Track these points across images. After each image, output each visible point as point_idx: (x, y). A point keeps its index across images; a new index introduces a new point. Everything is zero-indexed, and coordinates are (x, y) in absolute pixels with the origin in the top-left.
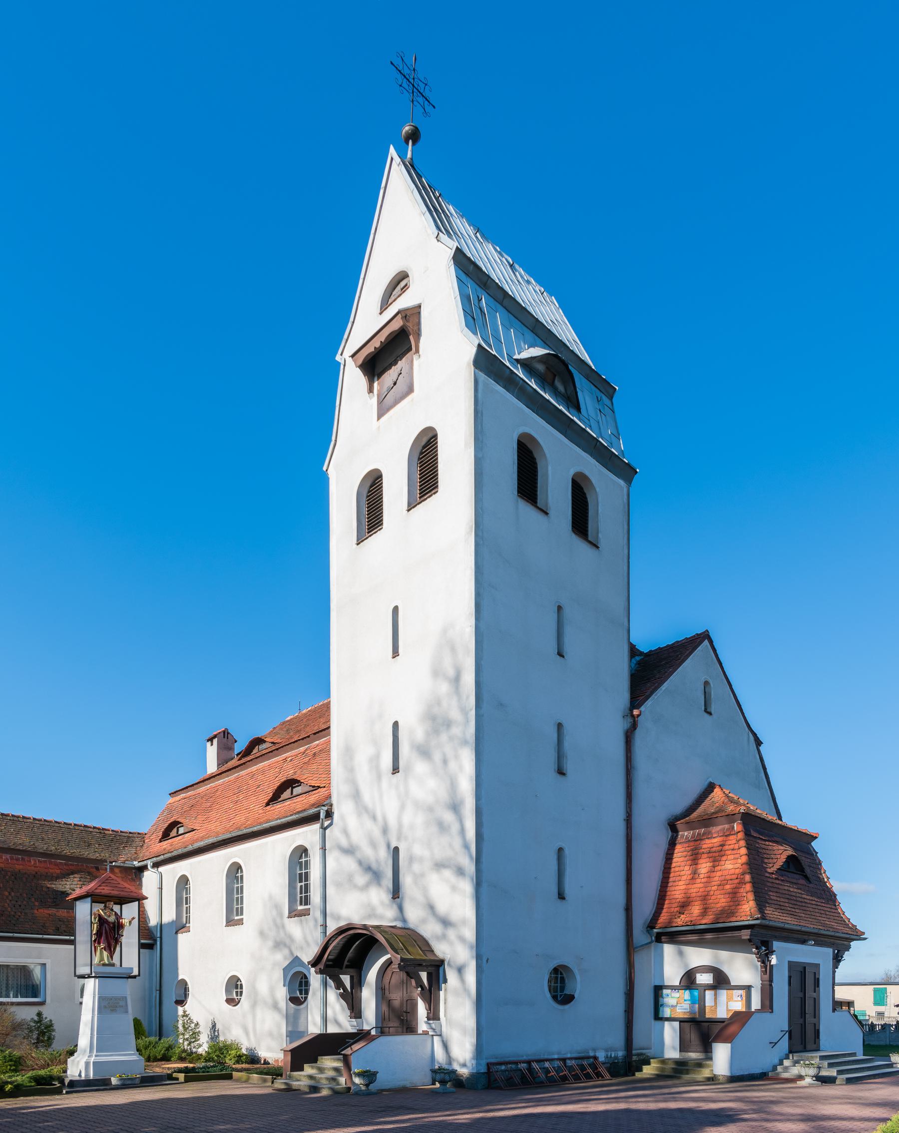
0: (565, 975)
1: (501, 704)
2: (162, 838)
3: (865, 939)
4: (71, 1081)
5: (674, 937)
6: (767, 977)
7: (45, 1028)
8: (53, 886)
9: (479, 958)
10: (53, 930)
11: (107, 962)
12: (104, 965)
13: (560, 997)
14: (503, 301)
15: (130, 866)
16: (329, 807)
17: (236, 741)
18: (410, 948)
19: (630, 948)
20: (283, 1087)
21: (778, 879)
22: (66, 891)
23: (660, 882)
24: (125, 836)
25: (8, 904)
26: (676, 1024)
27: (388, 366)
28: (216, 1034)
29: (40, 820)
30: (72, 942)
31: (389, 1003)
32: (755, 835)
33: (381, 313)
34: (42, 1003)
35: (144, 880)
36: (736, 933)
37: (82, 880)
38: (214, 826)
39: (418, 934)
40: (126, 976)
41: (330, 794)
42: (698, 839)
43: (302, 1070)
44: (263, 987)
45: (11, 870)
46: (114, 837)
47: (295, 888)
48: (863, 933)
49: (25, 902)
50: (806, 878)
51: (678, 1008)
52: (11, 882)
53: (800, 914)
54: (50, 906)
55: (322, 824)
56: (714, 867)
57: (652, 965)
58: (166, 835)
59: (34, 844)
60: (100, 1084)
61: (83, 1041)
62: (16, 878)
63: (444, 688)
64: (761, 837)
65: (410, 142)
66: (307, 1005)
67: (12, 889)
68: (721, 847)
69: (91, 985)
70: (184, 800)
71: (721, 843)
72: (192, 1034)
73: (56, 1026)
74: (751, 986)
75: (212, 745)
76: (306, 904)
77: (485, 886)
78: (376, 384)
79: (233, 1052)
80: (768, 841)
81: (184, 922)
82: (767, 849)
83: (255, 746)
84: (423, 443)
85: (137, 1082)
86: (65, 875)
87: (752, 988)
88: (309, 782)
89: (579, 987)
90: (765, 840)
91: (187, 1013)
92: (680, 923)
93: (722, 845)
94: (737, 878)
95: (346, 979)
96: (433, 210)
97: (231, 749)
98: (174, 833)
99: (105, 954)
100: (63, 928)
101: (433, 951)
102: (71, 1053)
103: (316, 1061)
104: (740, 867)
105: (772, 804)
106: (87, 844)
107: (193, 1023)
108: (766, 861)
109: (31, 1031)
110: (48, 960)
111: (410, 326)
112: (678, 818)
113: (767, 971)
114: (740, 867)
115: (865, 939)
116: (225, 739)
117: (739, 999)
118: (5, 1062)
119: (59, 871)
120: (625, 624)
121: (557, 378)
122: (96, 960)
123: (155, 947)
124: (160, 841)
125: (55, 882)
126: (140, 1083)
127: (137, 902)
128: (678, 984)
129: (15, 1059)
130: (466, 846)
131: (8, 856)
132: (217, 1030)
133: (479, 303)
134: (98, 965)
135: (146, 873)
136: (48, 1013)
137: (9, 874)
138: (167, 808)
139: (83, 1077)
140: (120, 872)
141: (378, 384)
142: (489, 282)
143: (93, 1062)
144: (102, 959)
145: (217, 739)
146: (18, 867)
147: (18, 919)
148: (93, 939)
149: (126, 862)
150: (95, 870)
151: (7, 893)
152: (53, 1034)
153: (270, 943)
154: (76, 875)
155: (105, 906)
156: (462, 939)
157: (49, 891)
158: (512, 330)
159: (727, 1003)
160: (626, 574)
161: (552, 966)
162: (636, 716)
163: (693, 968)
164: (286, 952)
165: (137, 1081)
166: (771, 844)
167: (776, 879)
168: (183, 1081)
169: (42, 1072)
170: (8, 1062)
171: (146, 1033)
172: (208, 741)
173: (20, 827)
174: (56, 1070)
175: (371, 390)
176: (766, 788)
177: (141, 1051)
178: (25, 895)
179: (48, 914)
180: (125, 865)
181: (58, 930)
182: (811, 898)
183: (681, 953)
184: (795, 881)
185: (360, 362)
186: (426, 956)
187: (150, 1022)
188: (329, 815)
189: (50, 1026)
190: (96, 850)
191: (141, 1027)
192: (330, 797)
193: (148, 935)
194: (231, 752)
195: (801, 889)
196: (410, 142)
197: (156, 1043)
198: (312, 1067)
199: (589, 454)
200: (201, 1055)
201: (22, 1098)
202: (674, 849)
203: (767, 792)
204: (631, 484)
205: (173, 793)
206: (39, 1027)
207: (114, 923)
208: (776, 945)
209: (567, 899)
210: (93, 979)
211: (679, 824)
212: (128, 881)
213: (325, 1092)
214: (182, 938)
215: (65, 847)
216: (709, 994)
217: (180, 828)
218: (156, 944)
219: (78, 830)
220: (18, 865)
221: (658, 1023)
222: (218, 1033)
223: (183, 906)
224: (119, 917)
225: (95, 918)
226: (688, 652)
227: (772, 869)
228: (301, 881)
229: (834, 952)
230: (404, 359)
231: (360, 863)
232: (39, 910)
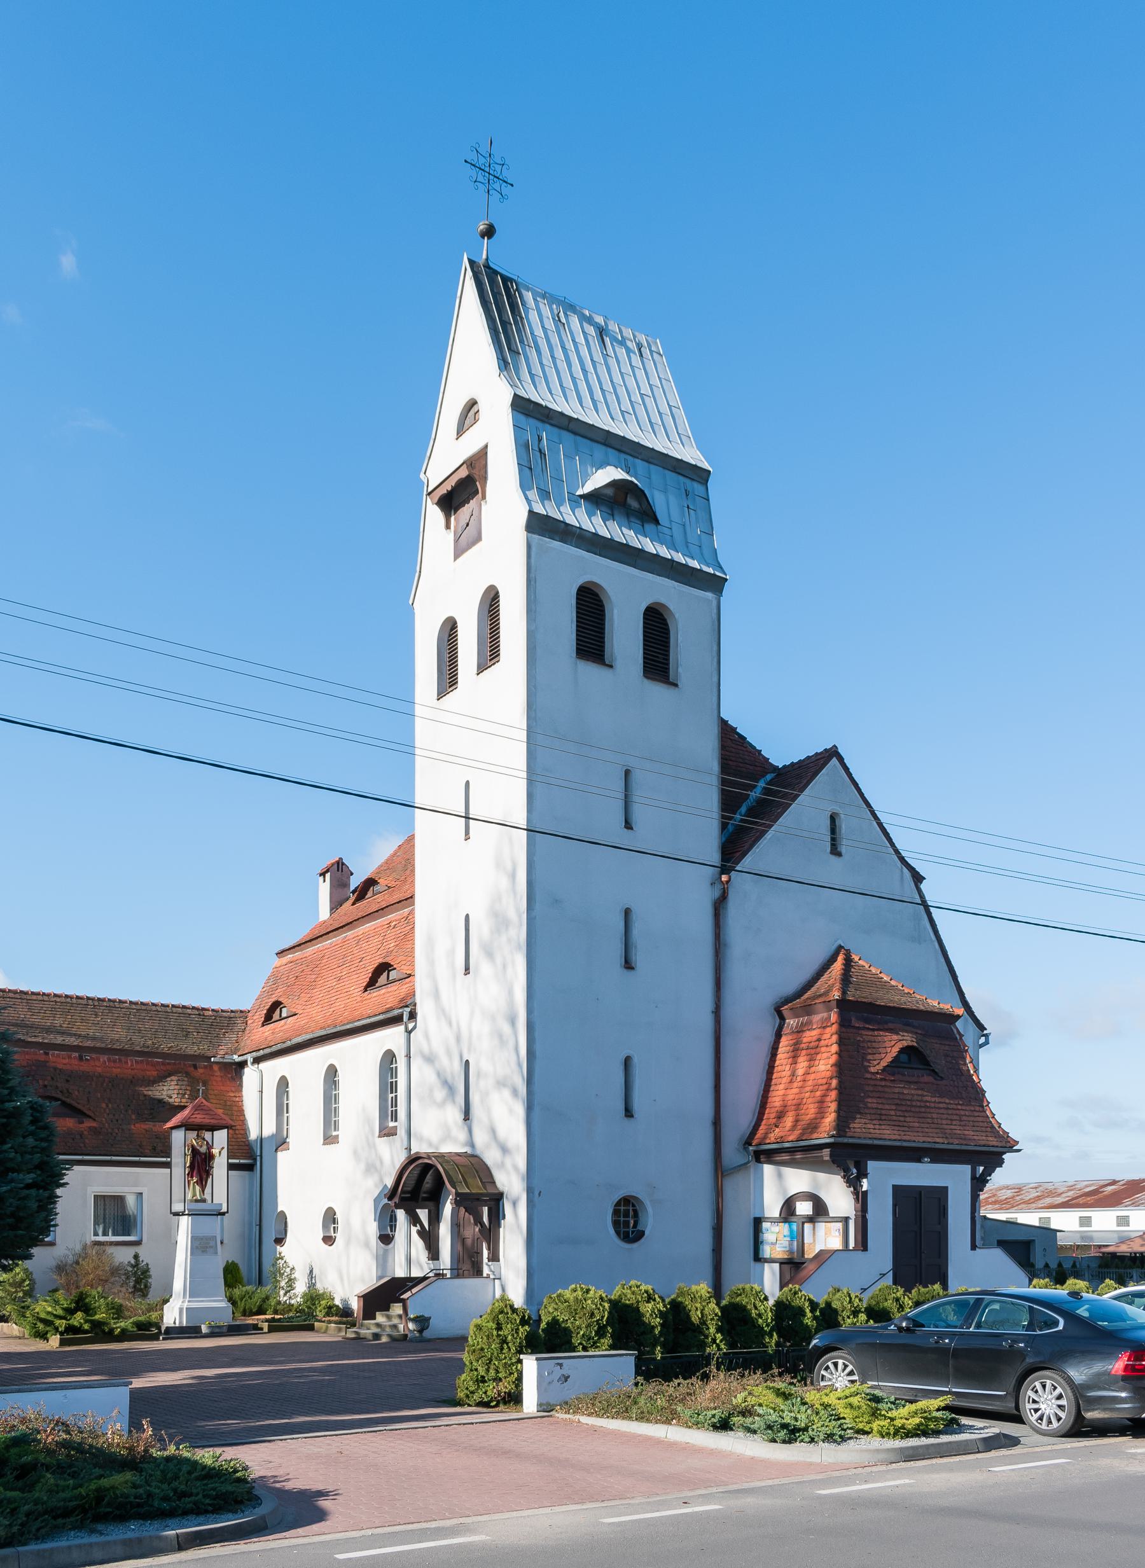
0: (638, 1208)
1: (557, 901)
2: (265, 1021)
3: (1019, 1151)
4: (167, 1328)
5: (765, 1155)
6: (859, 1205)
7: (142, 1274)
8: (150, 1093)
9: (530, 1190)
10: (150, 1150)
11: (199, 1198)
12: (197, 1201)
13: (632, 1234)
14: (569, 425)
15: (230, 1061)
16: (413, 1007)
17: (352, 874)
18: (469, 1180)
19: (720, 1171)
20: (353, 1336)
21: (885, 1080)
22: (163, 1099)
23: (763, 1085)
24: (226, 1017)
25: (106, 1119)
26: (776, 1266)
27: (462, 502)
28: (313, 1281)
29: (136, 1003)
30: (168, 1165)
31: (463, 1240)
32: (858, 1025)
33: (457, 439)
34: (138, 1243)
35: (245, 1078)
36: (816, 1154)
37: (180, 1083)
38: (315, 1011)
39: (484, 1162)
40: (215, 1213)
41: (414, 991)
42: (799, 1031)
43: (374, 1318)
44: (356, 1223)
45: (108, 1075)
46: (215, 1019)
47: (386, 1100)
48: (1017, 1143)
49: (122, 1115)
50: (934, 1072)
51: (777, 1245)
52: (108, 1090)
53: (911, 1124)
54: (147, 1120)
55: (406, 1028)
56: (810, 1067)
57: (752, 1191)
58: (268, 1018)
59: (131, 1038)
60: (191, 1331)
61: (178, 1285)
62: (113, 1086)
63: (504, 882)
64: (867, 1026)
65: (486, 238)
66: (394, 1245)
67: (109, 1100)
68: (817, 1042)
69: (185, 1222)
70: (291, 965)
71: (818, 1037)
72: (288, 1282)
73: (152, 1272)
74: (849, 1217)
75: (324, 881)
76: (396, 1121)
77: (537, 1109)
78: (453, 518)
79: (323, 1303)
80: (878, 1030)
81: (285, 1136)
82: (875, 1042)
83: (370, 888)
84: (492, 596)
85: (224, 1331)
86: (162, 1078)
87: (850, 1220)
88: (402, 967)
89: (650, 1223)
90: (873, 1030)
91: (282, 1255)
92: (773, 1139)
93: (819, 1040)
94: (826, 1083)
95: (423, 1214)
96: (501, 331)
97: (346, 885)
98: (276, 1016)
99: (198, 1188)
100: (159, 1148)
101: (494, 1183)
102: (166, 1301)
103: (388, 1309)
104: (831, 1069)
105: (943, 960)
106: (184, 1033)
107: (288, 1267)
108: (870, 1057)
109: (128, 1278)
110: (144, 1188)
111: (476, 474)
112: (788, 1000)
113: (862, 1199)
114: (831, 1069)
115: (1019, 1151)
116: (338, 871)
117: (837, 1234)
118: (108, 1310)
119: (156, 1073)
120: (713, 768)
121: (629, 496)
122: (189, 1196)
123: (255, 1168)
124: (263, 1026)
125: (151, 1088)
126: (228, 1331)
127: (226, 1130)
128: (778, 1216)
129: (116, 1307)
130: (520, 1065)
131: (106, 1058)
132: (314, 1276)
133: (539, 444)
134: (191, 1201)
135: (246, 1070)
136: (146, 1256)
137: (107, 1080)
138: (273, 974)
139: (177, 1325)
140: (220, 1069)
141: (455, 519)
142: (551, 414)
143: (186, 1308)
144: (194, 1195)
145: (329, 873)
146: (116, 1071)
147: (115, 1137)
148: (187, 1173)
149: (226, 1056)
150: (192, 1069)
151: (104, 1105)
152: (150, 1280)
153: (362, 1166)
154: (173, 1078)
155: (198, 1135)
156: (516, 1168)
157: (146, 1099)
158: (577, 458)
159: (826, 1239)
160: (715, 706)
161: (616, 1197)
162: (724, 882)
163: (795, 1194)
164: (376, 1178)
165: (225, 1330)
166: (881, 1033)
167: (881, 1079)
168: (267, 1331)
169: (142, 1318)
170: (111, 1309)
171: (245, 1280)
172: (320, 875)
173: (117, 1015)
174: (153, 1316)
175: (448, 527)
176: (931, 939)
177: (237, 1303)
178: (122, 1107)
179: (144, 1129)
180: (225, 1061)
181: (155, 1149)
182: (940, 1100)
183: (780, 1176)
184: (914, 1079)
185: (436, 500)
186: (486, 1189)
187: (250, 1271)
188: (413, 1016)
189: (146, 1272)
190: (194, 1041)
191: (239, 1273)
192: (414, 995)
193: (248, 1153)
194: (346, 889)
195: (922, 1089)
196: (486, 238)
197: (253, 1293)
198: (383, 1315)
199: (666, 577)
200: (293, 1305)
201: (126, 1343)
202: (780, 1042)
203: (934, 946)
204: (722, 593)
205: (279, 953)
206: (136, 1272)
207: (205, 1154)
208: (872, 1165)
209: (636, 1116)
210: (187, 1216)
211: (785, 1009)
212: (228, 1080)
213: (384, 1339)
214: (281, 1156)
215: (162, 1039)
216: (807, 1226)
217: (283, 1009)
218: (256, 1164)
219: (175, 1013)
220: (115, 1068)
221: (758, 1265)
222: (315, 1280)
223: (283, 1115)
224: (210, 1147)
225: (188, 1150)
226: (805, 781)
227: (877, 1067)
228: (392, 1093)
229: (974, 1171)
230: (475, 499)
231: (438, 1074)
232: (136, 1125)
